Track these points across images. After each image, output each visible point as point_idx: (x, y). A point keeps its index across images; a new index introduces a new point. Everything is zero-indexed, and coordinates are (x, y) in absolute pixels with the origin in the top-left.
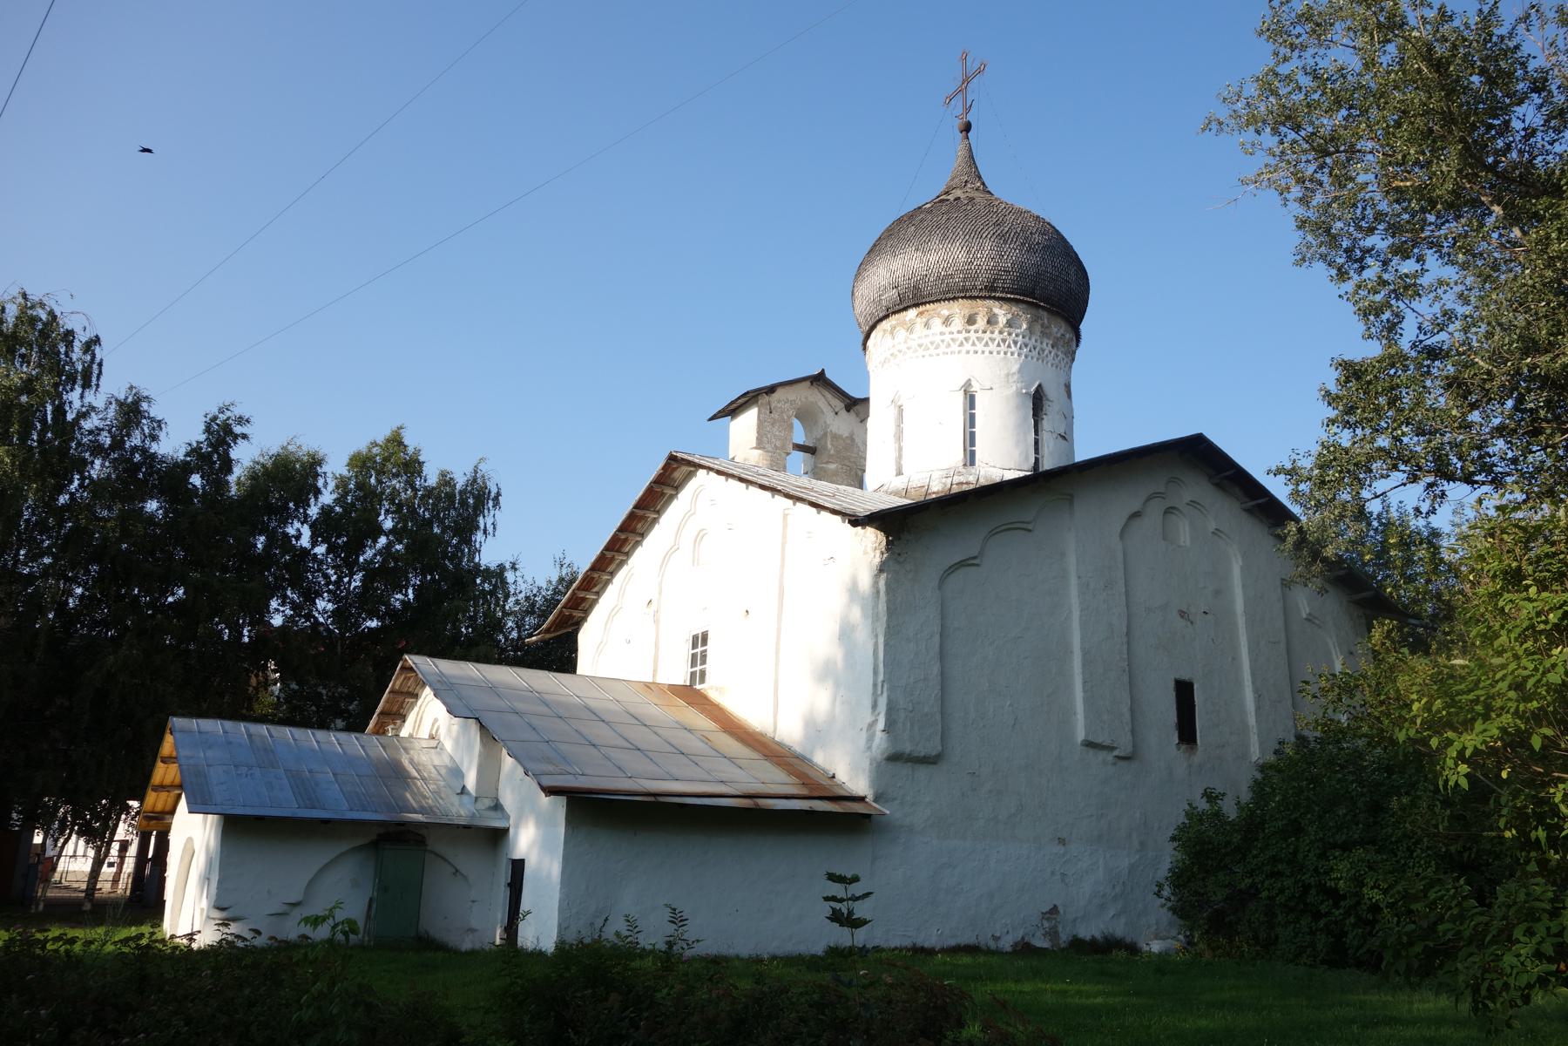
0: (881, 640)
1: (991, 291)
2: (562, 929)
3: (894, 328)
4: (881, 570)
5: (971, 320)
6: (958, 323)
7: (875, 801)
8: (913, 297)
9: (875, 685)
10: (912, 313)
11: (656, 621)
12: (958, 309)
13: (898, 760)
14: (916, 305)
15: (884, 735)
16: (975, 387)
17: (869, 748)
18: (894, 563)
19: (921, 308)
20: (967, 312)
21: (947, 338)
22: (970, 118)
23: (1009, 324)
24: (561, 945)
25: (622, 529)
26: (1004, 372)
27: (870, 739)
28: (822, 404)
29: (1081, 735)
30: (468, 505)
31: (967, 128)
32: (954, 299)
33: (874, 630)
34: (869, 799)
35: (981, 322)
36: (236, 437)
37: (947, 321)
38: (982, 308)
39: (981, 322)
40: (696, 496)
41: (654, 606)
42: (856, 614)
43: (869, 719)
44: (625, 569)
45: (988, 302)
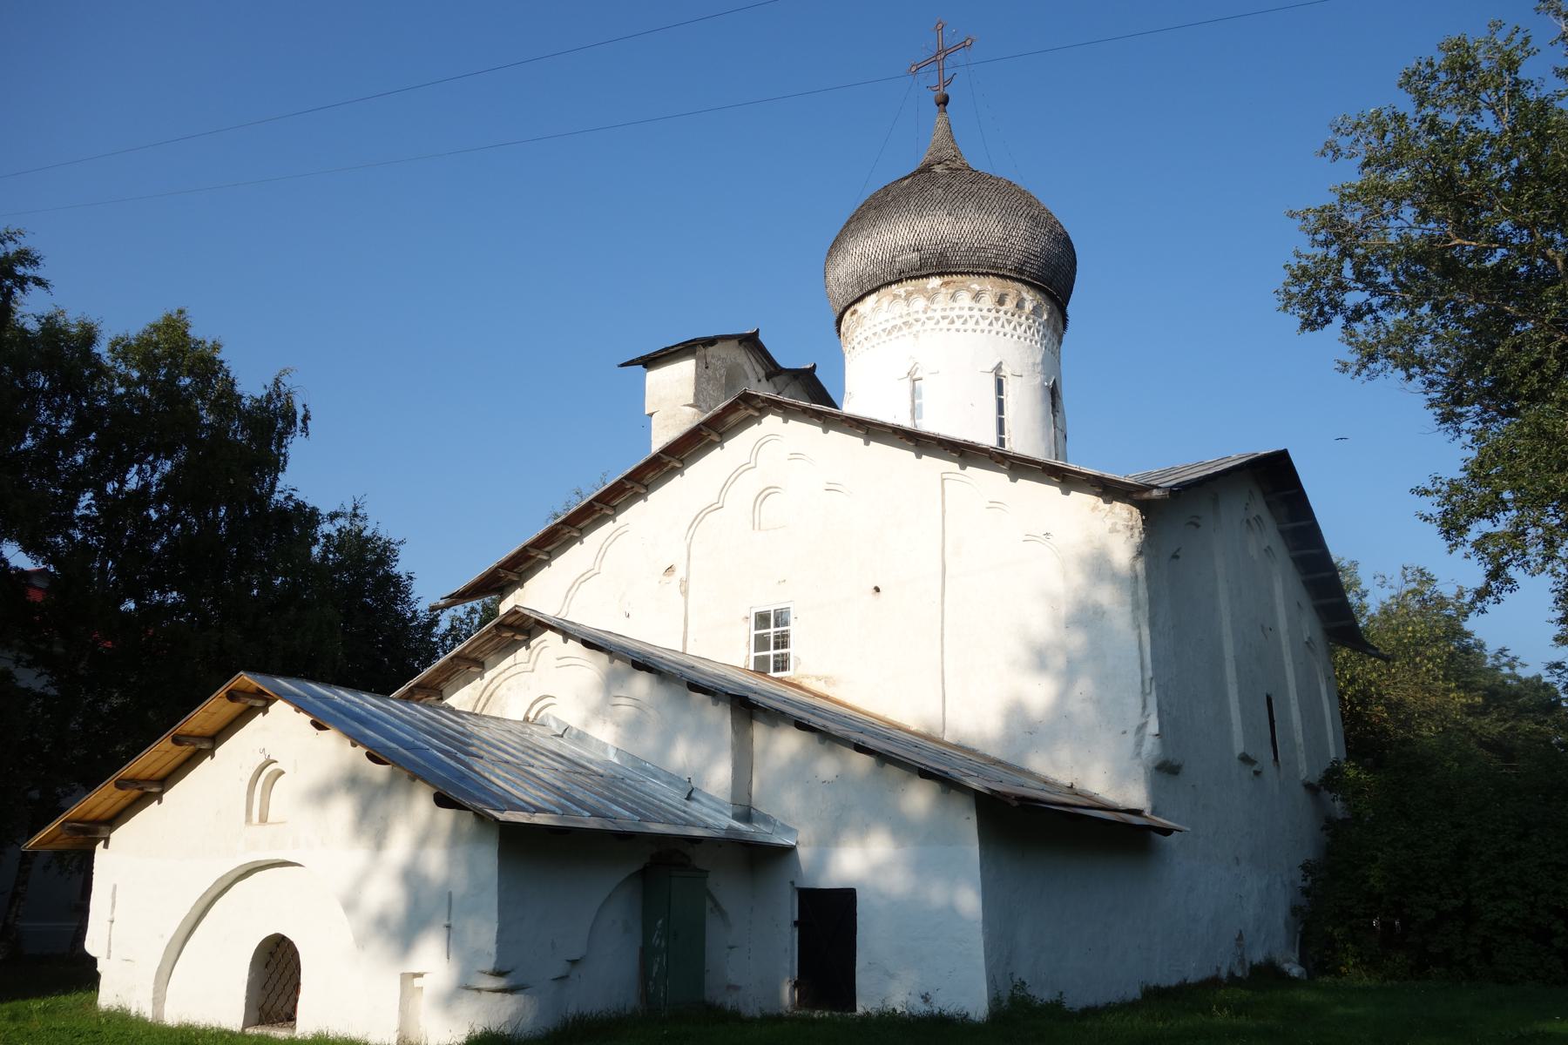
0: (1146, 632)
1: (1019, 274)
2: (992, 982)
3: (909, 295)
4: (1140, 553)
5: (1001, 301)
6: (988, 301)
7: (1153, 813)
8: (938, 264)
9: (1143, 682)
10: (935, 282)
11: (685, 593)
12: (990, 286)
13: (1166, 770)
14: (941, 274)
15: (1156, 740)
16: (1006, 371)
17: (1139, 754)
18: (1150, 547)
19: (946, 278)
20: (998, 291)
21: (976, 312)
22: (947, 91)
23: (1035, 311)
24: (995, 1001)
25: (628, 477)
26: (1031, 361)
27: (1139, 744)
28: (747, 367)
29: (1239, 747)
30: (273, 423)
31: (944, 102)
32: (987, 274)
33: (1135, 619)
34: (1147, 814)
35: (1010, 304)
36: (22, 282)
37: (977, 296)
38: (1013, 288)
39: (1010, 304)
40: (760, 444)
41: (680, 573)
42: (1106, 596)
43: (1138, 722)
44: (608, 527)
45: (1018, 285)
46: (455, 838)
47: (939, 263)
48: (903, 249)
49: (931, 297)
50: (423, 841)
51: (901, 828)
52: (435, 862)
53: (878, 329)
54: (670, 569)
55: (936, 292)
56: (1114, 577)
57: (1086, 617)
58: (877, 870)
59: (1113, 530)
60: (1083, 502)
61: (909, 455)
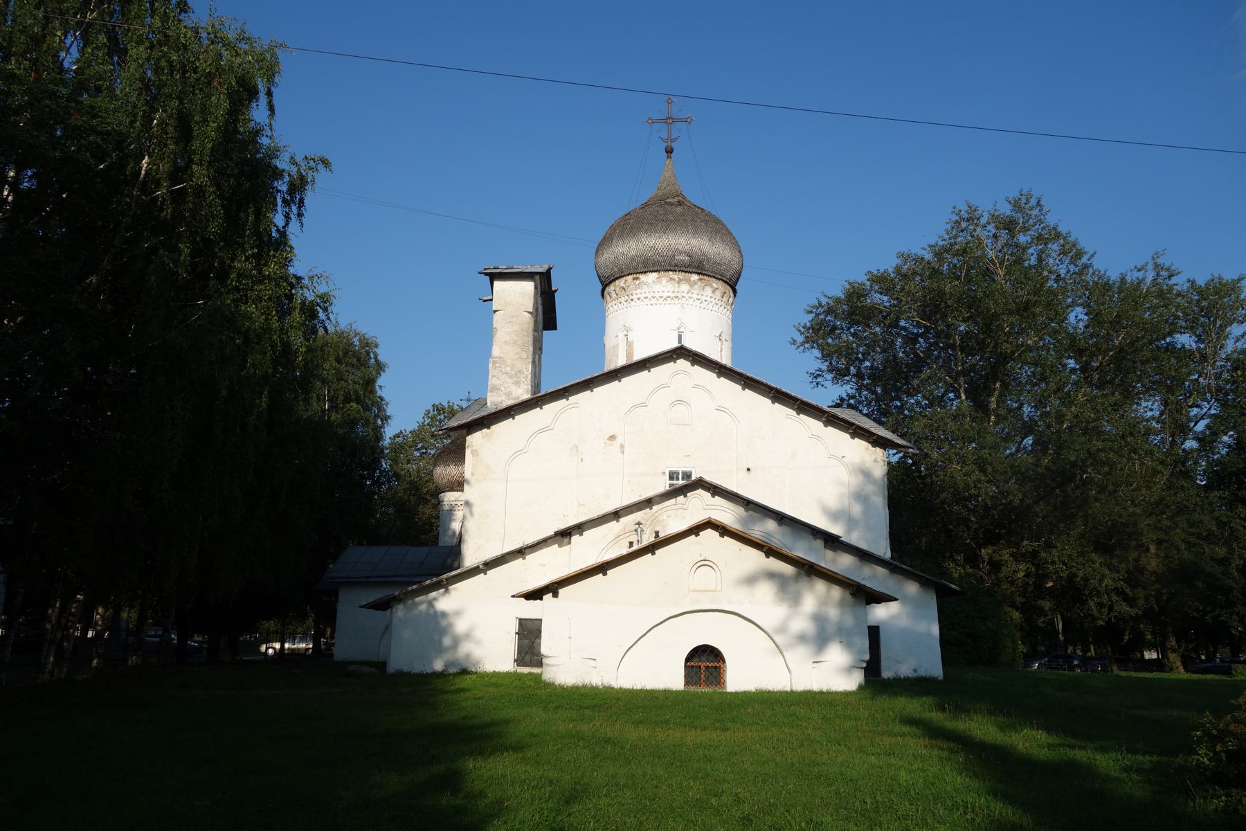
3: (680, 281)
6: (718, 294)
8: (697, 267)
10: (695, 277)
22: (673, 145)
31: (669, 151)
42: (870, 488)
46: (842, 604)
47: (698, 267)
48: (681, 253)
49: (692, 284)
50: (823, 603)
51: (906, 600)
52: (833, 613)
53: (657, 295)
54: (612, 438)
55: (695, 283)
56: (874, 482)
57: (860, 497)
58: (893, 617)
59: (876, 461)
60: (860, 445)
61: (768, 401)
